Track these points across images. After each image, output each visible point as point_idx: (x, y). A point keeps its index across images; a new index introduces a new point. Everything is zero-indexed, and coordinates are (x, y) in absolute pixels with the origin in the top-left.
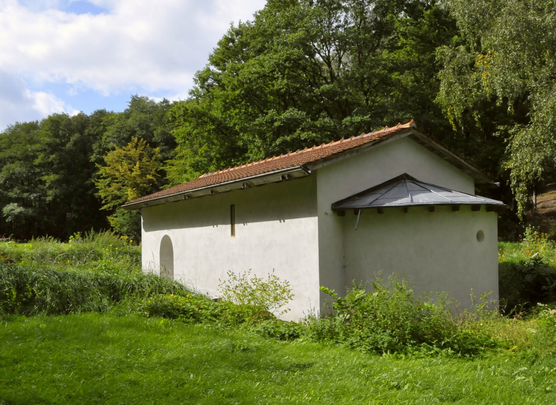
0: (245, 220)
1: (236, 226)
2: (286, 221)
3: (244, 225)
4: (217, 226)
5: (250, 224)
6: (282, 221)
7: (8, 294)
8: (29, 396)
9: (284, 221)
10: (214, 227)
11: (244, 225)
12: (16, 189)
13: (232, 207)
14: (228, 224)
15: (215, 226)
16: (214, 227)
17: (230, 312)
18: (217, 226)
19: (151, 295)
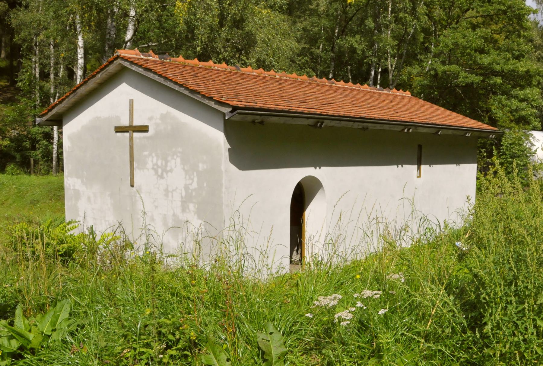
0: (431, 162)
1: (423, 167)
2: (322, 168)
3: (430, 166)
4: (402, 166)
5: (462, 166)
6: (318, 168)
7: (218, 311)
8: (527, 144)
9: (320, 168)
10: (398, 167)
11: (430, 166)
12: (376, 59)
13: (420, 147)
14: (416, 165)
15: (400, 166)
16: (398, 167)
17: (493, 175)
18: (402, 166)
19: (181, 351)
